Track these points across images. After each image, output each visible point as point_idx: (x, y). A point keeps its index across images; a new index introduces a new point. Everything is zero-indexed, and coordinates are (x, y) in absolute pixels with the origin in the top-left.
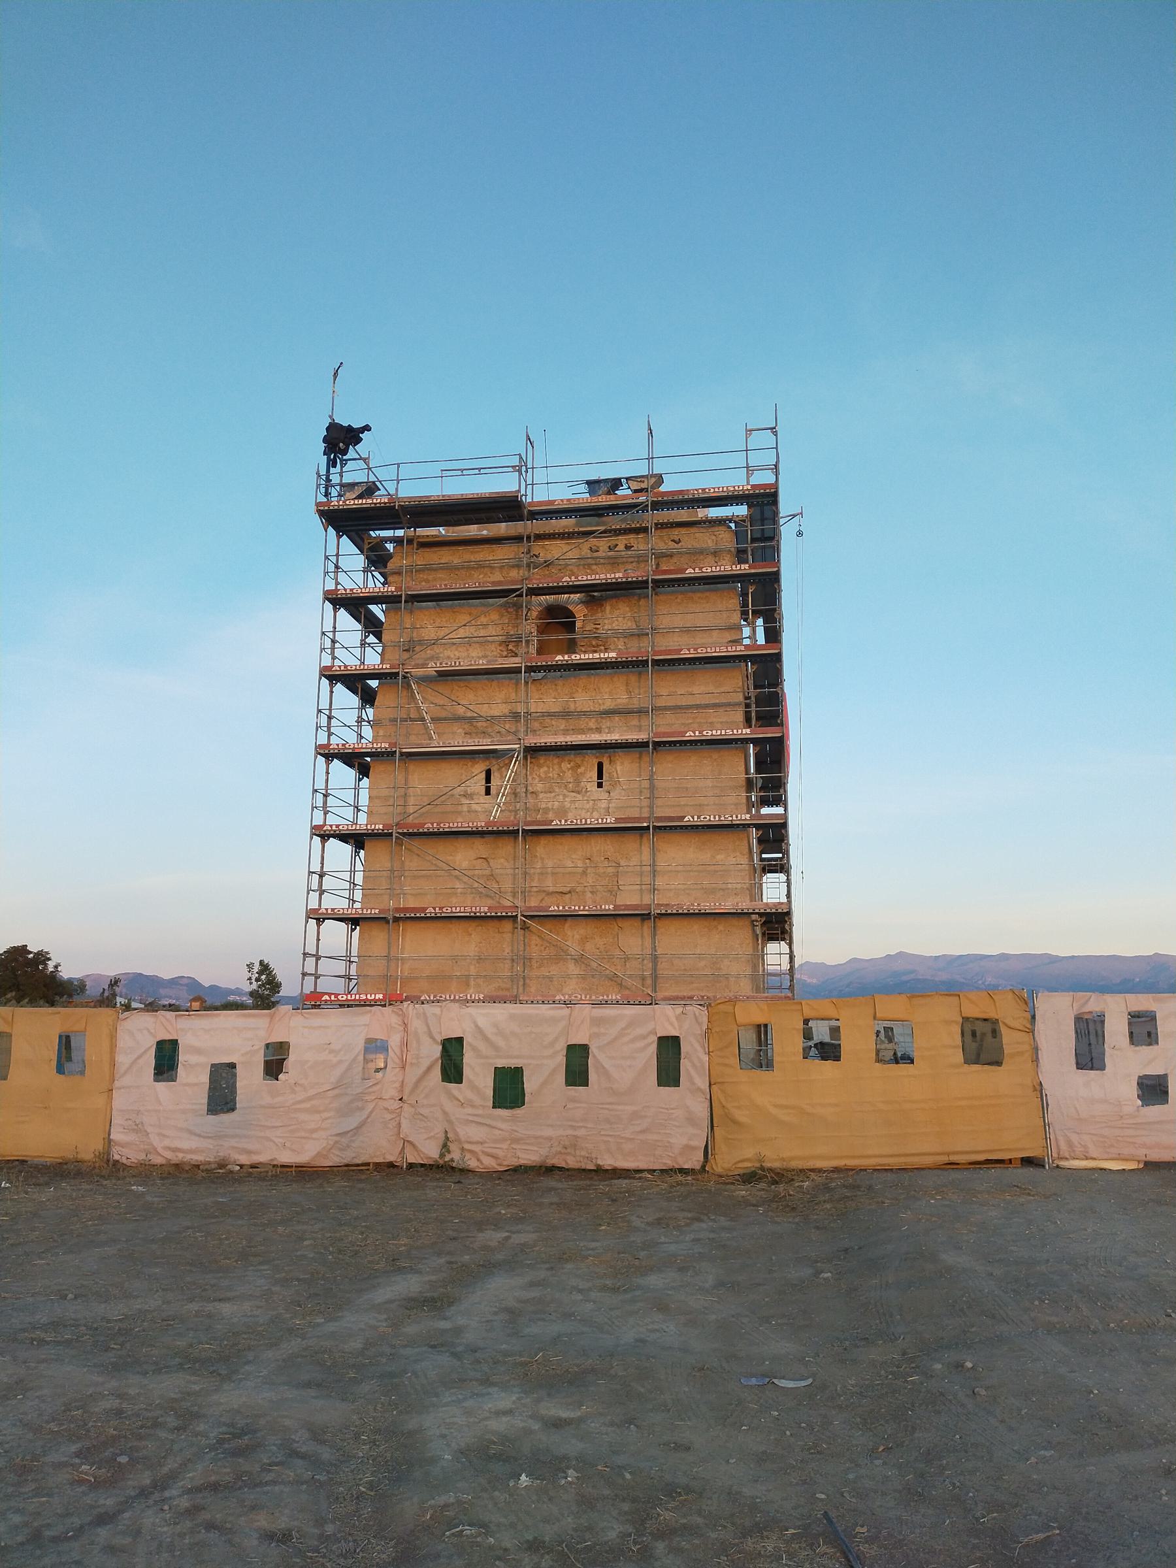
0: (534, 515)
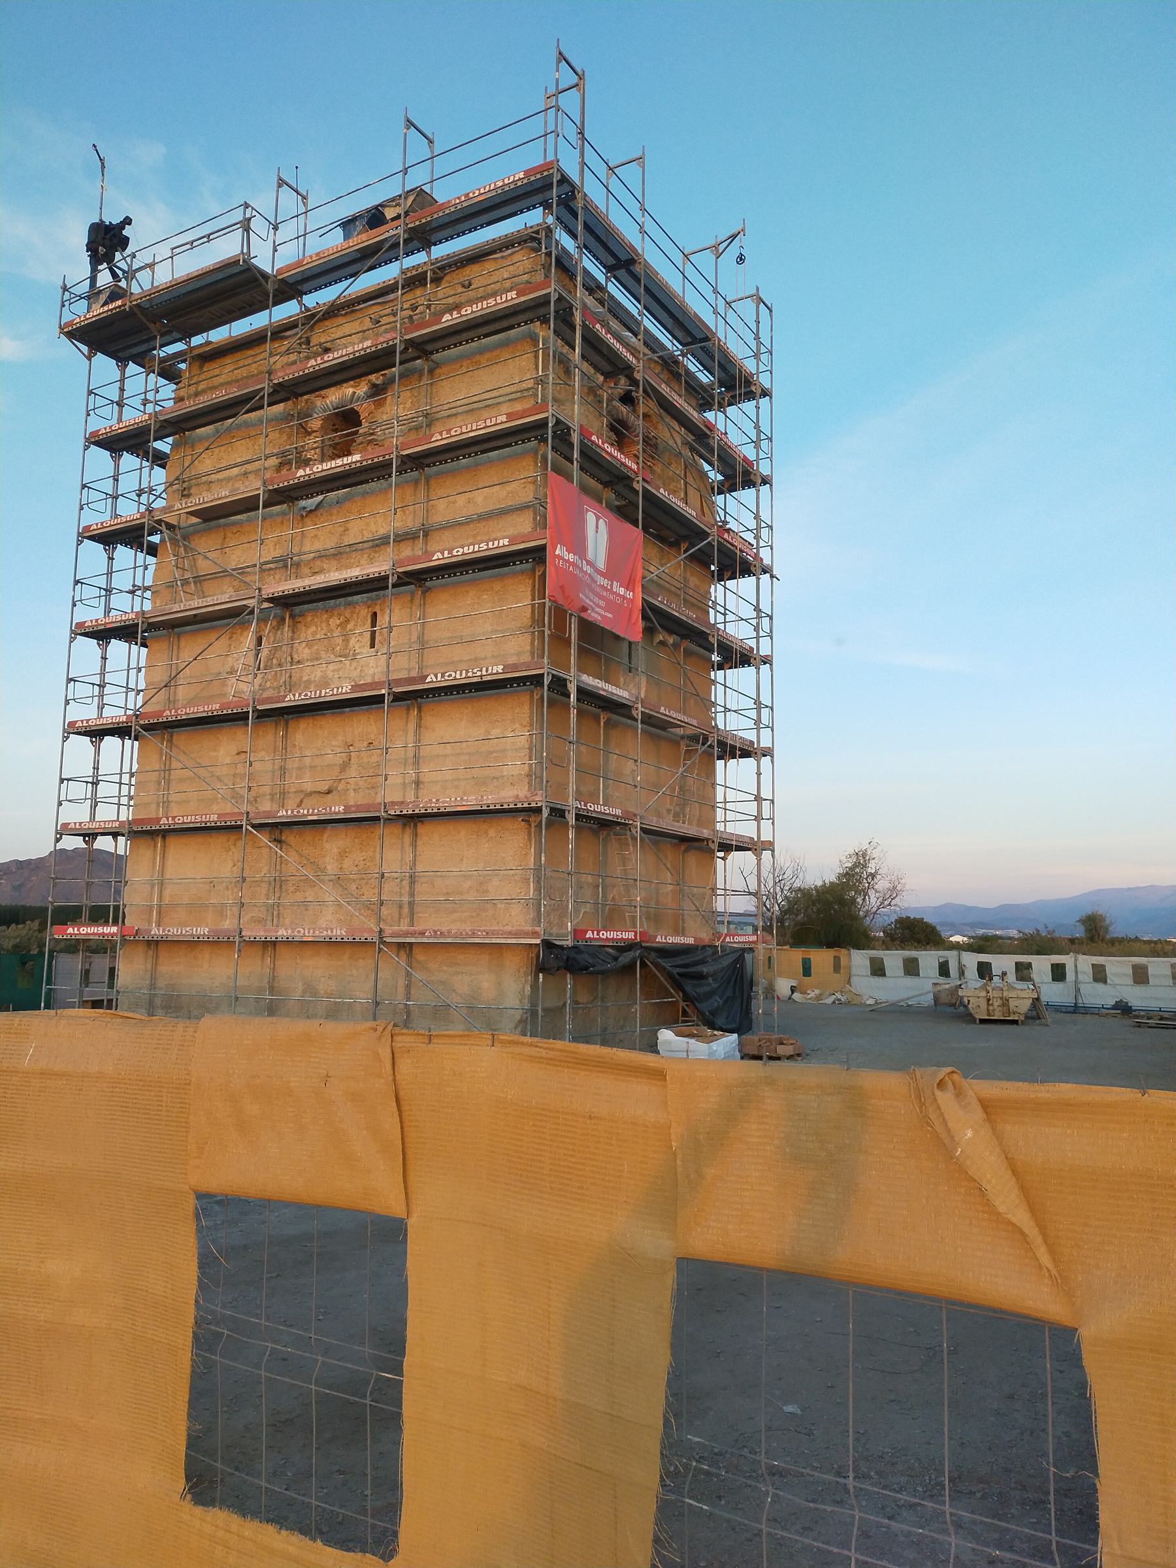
0: (291, 287)
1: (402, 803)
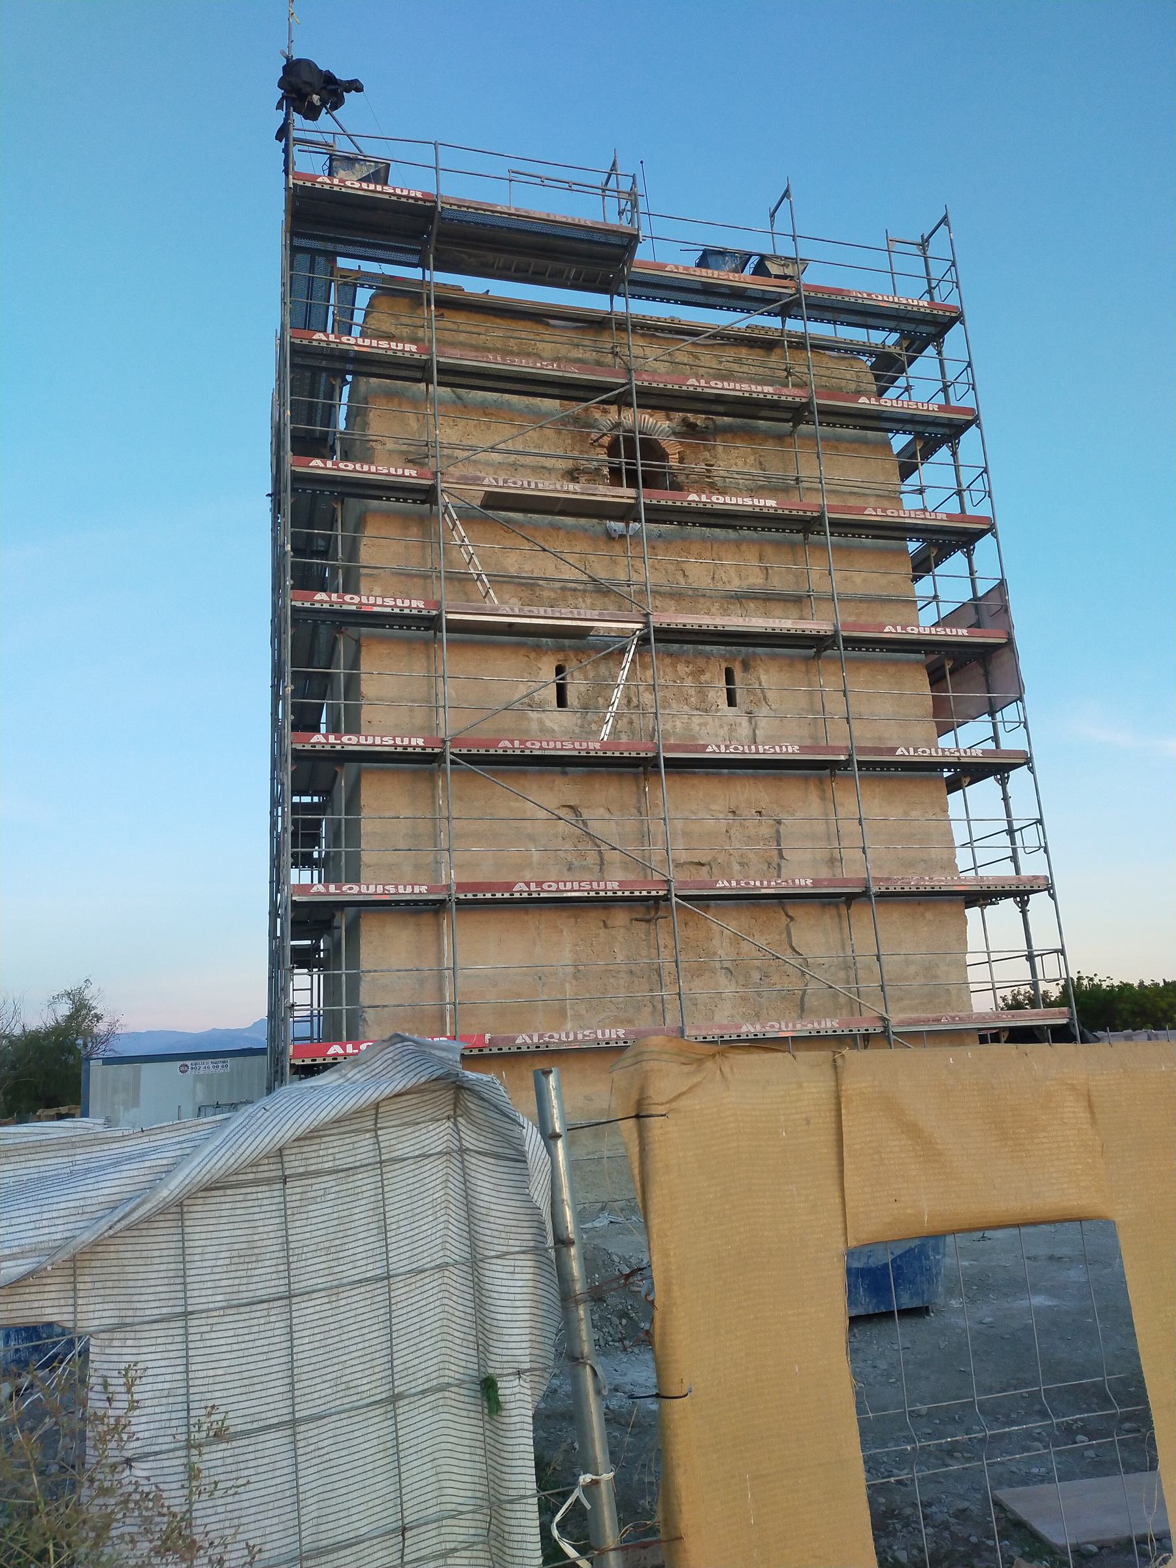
1: (888, 879)
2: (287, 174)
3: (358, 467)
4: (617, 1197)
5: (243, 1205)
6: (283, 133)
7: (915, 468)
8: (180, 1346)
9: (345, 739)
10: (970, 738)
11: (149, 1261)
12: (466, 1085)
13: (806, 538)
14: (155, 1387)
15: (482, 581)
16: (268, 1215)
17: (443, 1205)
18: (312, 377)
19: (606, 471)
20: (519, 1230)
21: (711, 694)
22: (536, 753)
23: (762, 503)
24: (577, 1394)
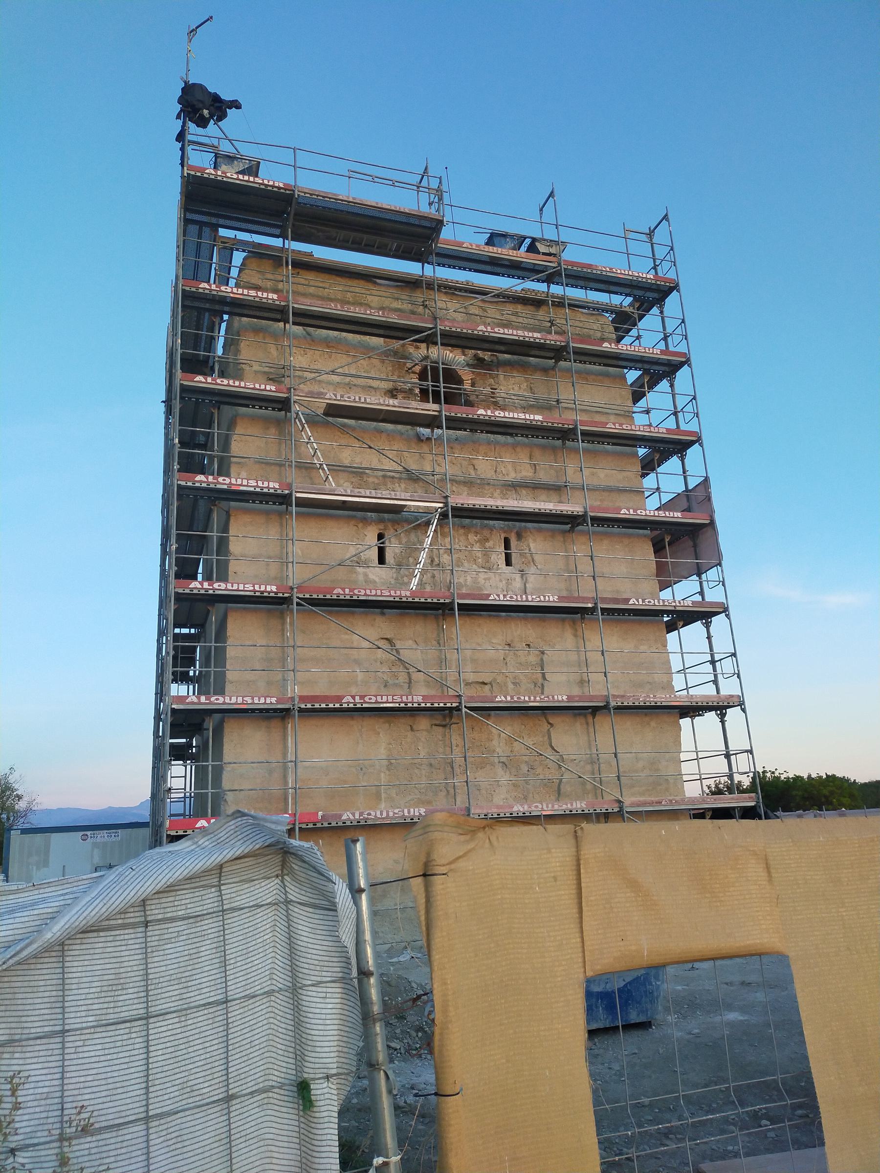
1: (623, 696)
2: (183, 166)
3: (231, 382)
4: (417, 938)
5: (113, 944)
6: (181, 137)
7: (643, 395)
8: (58, 1058)
9: (216, 586)
10: (683, 593)
11: (35, 989)
12: (291, 851)
13: (564, 444)
14: (37, 1091)
15: (323, 469)
16: (132, 952)
17: (272, 945)
18: (197, 314)
19: (417, 391)
20: (331, 964)
21: (494, 557)
22: (361, 598)
23: (532, 417)
24: (372, 1093)
